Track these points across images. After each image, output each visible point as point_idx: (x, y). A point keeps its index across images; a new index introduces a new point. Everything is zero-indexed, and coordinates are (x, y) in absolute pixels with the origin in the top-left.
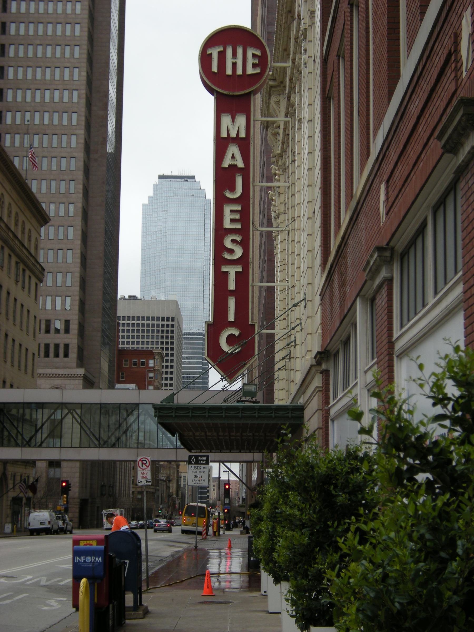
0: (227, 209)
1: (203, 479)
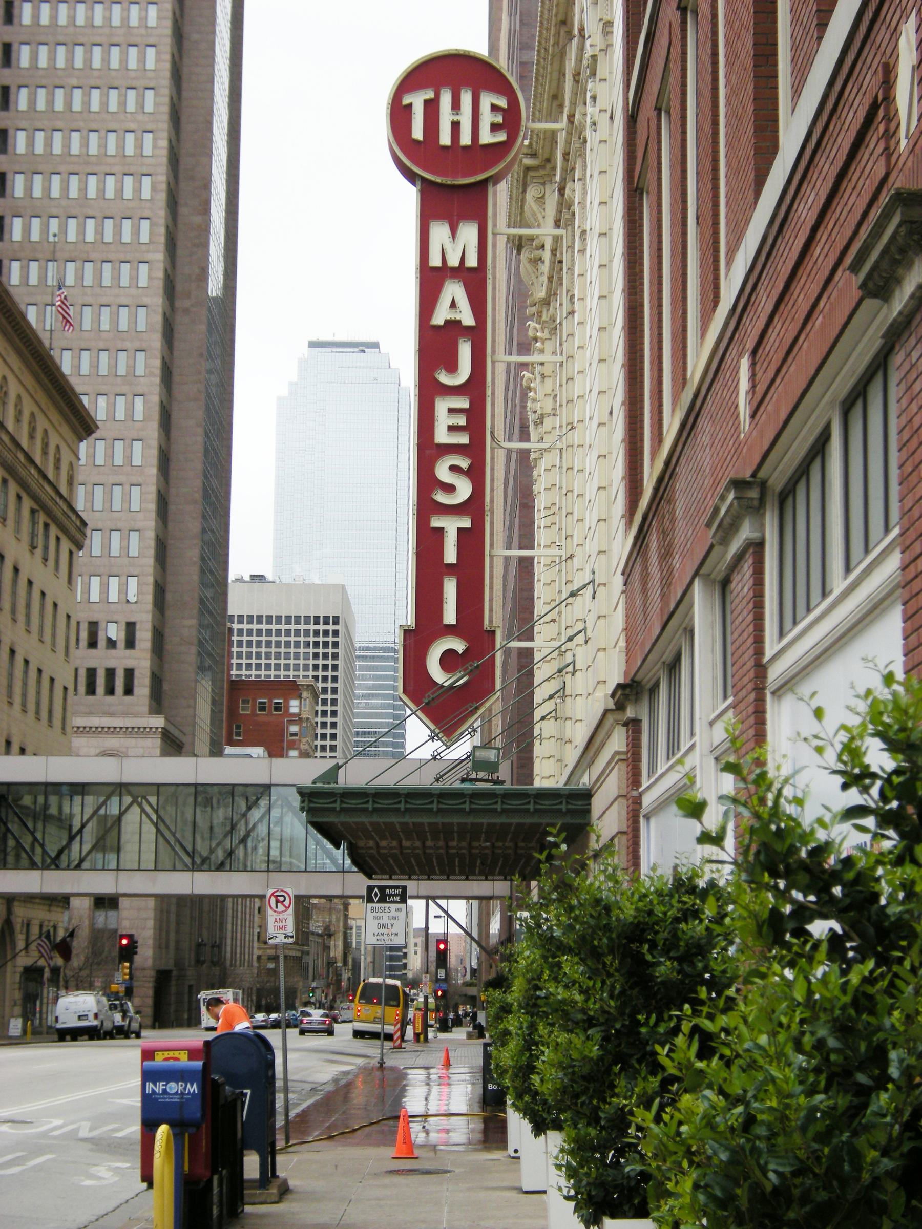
0: (442, 406)
1: (394, 931)
